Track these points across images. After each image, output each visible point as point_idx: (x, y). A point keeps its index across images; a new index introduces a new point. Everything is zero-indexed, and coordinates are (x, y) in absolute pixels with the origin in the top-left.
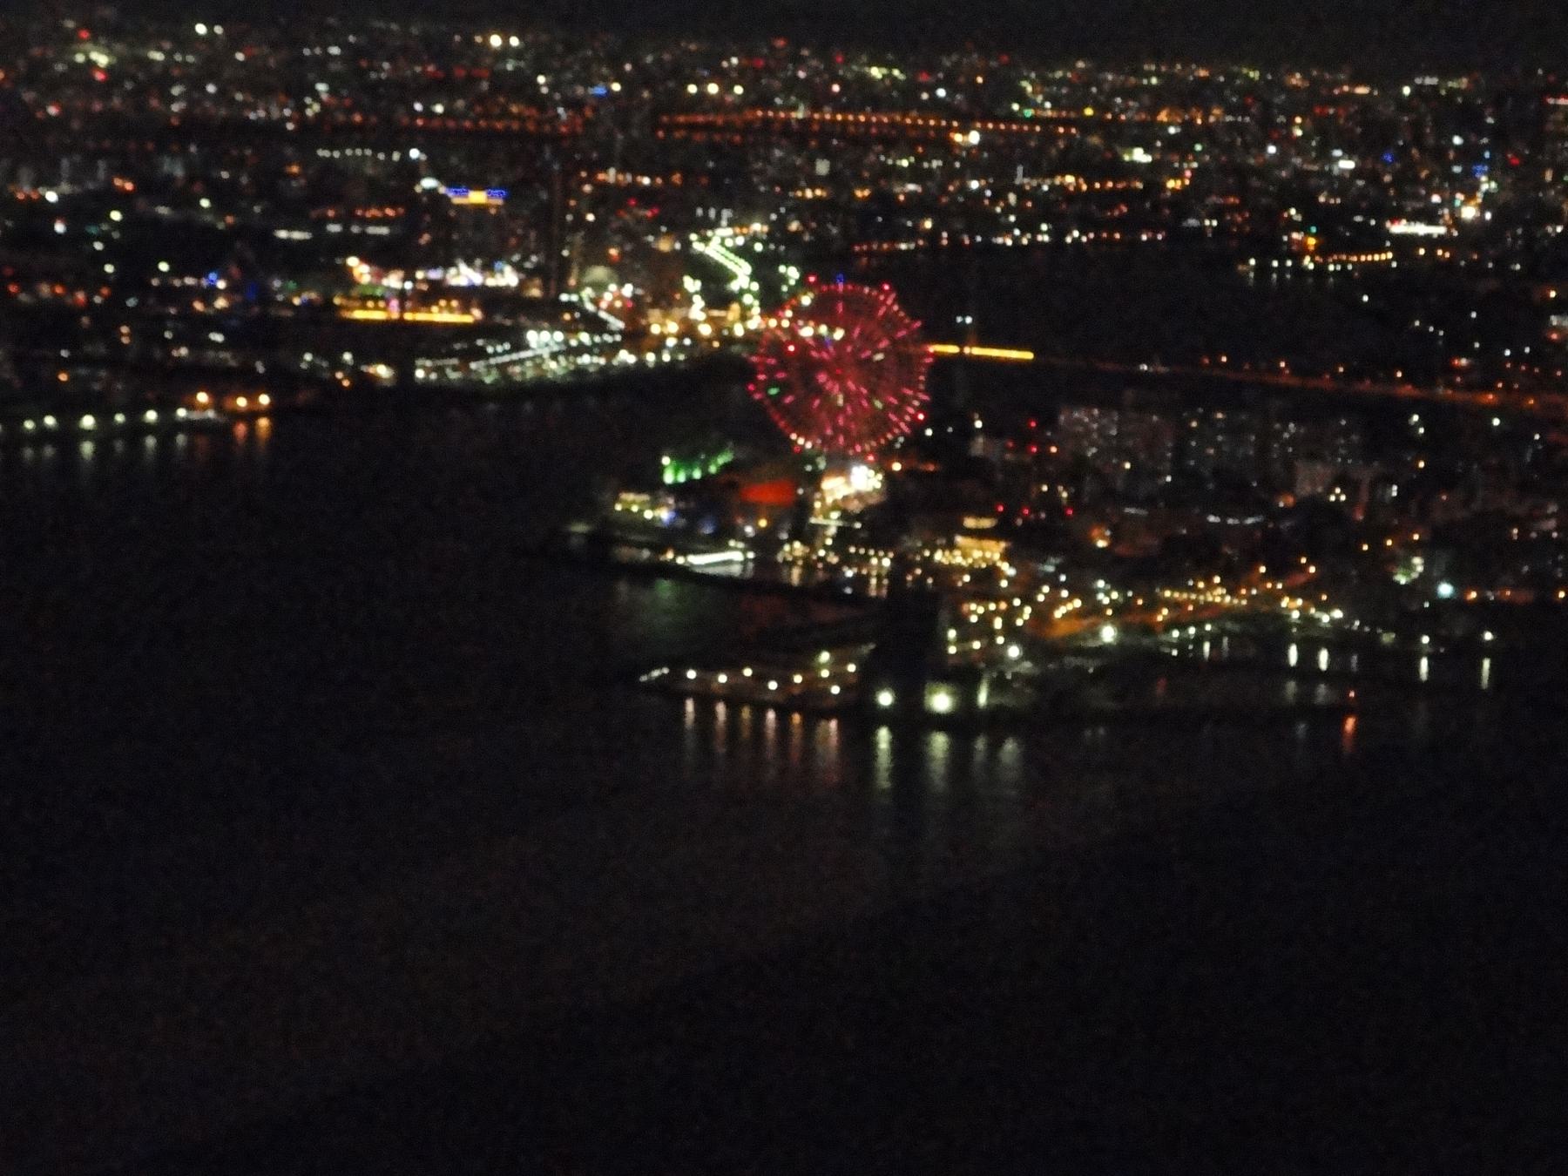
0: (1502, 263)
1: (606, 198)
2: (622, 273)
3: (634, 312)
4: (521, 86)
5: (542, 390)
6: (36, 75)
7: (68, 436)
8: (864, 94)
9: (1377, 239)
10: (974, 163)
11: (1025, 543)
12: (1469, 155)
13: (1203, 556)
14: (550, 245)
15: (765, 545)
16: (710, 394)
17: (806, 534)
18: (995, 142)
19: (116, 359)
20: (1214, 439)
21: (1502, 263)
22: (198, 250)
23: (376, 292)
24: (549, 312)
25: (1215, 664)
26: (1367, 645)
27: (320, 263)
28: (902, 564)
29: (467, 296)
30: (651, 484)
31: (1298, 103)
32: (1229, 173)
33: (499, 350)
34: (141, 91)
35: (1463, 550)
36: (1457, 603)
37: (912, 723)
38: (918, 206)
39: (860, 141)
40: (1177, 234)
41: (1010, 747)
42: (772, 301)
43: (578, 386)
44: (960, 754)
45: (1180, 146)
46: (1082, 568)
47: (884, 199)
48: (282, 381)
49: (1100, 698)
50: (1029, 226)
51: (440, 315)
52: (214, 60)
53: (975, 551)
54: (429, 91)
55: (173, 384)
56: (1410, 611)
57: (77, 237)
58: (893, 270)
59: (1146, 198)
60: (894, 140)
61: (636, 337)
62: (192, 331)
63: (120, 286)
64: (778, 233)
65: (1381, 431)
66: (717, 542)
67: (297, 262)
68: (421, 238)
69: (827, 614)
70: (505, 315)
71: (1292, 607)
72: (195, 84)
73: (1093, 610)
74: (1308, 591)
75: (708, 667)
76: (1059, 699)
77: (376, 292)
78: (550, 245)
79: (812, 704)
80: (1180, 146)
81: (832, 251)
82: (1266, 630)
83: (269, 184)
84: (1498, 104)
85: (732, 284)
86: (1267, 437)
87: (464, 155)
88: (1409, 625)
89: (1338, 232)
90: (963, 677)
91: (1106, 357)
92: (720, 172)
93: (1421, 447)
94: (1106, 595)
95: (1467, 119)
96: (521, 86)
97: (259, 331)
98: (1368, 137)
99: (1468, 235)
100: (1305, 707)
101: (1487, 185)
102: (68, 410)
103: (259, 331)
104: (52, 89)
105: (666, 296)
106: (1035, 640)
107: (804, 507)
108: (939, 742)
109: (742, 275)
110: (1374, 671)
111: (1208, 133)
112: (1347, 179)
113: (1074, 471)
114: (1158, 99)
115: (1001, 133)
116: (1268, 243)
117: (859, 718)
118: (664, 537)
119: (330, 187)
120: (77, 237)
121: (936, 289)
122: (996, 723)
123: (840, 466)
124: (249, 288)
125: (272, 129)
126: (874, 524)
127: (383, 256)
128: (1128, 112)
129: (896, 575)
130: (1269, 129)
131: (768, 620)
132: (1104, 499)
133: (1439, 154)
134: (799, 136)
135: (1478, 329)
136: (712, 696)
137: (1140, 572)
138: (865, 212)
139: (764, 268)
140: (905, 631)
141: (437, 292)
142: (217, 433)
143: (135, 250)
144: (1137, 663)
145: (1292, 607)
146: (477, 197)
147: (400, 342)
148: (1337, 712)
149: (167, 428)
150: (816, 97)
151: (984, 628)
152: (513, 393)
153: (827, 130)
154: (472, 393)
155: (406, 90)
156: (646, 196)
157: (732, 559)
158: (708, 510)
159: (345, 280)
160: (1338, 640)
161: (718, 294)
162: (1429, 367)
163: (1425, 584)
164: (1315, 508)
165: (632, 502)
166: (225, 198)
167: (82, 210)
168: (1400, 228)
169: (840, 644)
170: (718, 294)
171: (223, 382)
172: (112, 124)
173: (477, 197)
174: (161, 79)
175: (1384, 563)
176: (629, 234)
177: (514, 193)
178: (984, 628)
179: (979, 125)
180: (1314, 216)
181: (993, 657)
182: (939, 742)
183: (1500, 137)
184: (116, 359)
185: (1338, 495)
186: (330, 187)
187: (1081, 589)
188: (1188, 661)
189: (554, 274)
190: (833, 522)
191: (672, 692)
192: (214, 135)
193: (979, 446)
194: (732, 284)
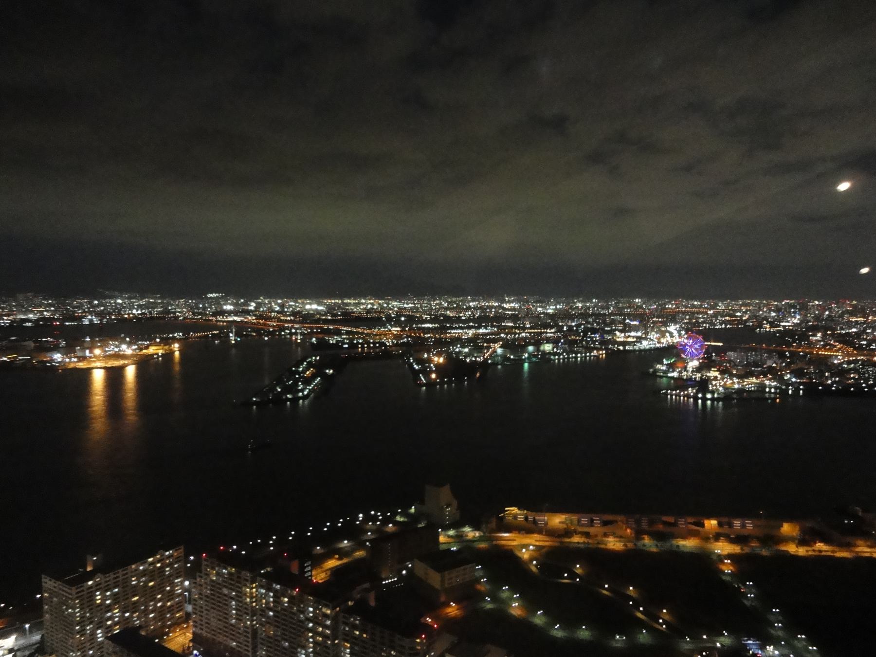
0: (802, 328)
1: (654, 322)
2: (657, 332)
3: (659, 339)
4: (641, 307)
5: (645, 350)
6: (571, 308)
7: (576, 358)
8: (693, 306)
9: (779, 326)
10: (712, 316)
11: (722, 372)
12: (795, 313)
13: (750, 374)
14: (646, 329)
15: (680, 372)
16: (672, 351)
17: (687, 371)
18: (719, 312)
19: (583, 346)
20: (752, 357)
21: (802, 328)
22: (594, 331)
23: (620, 337)
24: (646, 339)
25: (754, 391)
26: (780, 388)
27: (612, 332)
28: (702, 375)
29: (633, 337)
30: (662, 363)
31: (765, 306)
32: (754, 316)
33: (638, 345)
34: (585, 310)
35: (798, 373)
36: (796, 382)
37: (704, 400)
38: (703, 322)
39: (693, 313)
40: (746, 326)
41: (721, 403)
42: (680, 336)
43: (650, 350)
44: (712, 404)
45: (745, 312)
46: (731, 376)
47: (697, 322)
48: (607, 349)
49: (735, 396)
50: (721, 325)
51: (630, 339)
52: (596, 305)
53: (713, 373)
54: (628, 308)
55: (591, 350)
56: (788, 384)
57: (577, 330)
58: (699, 332)
59: (741, 321)
60: (699, 313)
61: (659, 342)
62: (594, 342)
63: (583, 337)
64: (681, 327)
65: (782, 356)
66: (673, 371)
67: (609, 332)
68: (626, 329)
69: (689, 383)
70: (639, 339)
71: (767, 382)
72: (593, 308)
73: (733, 383)
74: (770, 380)
75: (672, 390)
76: (728, 397)
77: (620, 337)
78: (646, 329)
79: (688, 396)
80: (745, 312)
81: (691, 329)
82: (762, 387)
83: (604, 322)
84: (799, 304)
85: (674, 335)
86: (762, 356)
87: (633, 317)
88: (788, 385)
89: (772, 325)
90: (713, 392)
91: (733, 343)
92: (672, 318)
93: (788, 358)
94: (735, 380)
95: (794, 307)
96: (641, 307)
97: (604, 343)
98: (778, 310)
99: (795, 325)
100: (770, 398)
101: (798, 317)
102: (576, 353)
103: (604, 343)
104: (573, 309)
105: (663, 336)
106: (724, 387)
107: (686, 367)
108: (709, 402)
109: (675, 333)
110: (783, 393)
111: (750, 310)
112: (773, 317)
113: (730, 361)
114: (741, 306)
115: (308, 640)
116: (760, 326)
117: (696, 398)
118: (665, 372)
119: (613, 322)
120: (577, 330)
121: (707, 335)
122: (718, 400)
123: (692, 360)
124: (602, 336)
125: (605, 314)
126: (699, 369)
127: (621, 331)
128: (737, 308)
129: (701, 378)
130: (760, 309)
131: (681, 384)
132: (735, 366)
133: (790, 313)
134: (684, 313)
135: (797, 339)
136: (673, 395)
137: (741, 377)
138: (695, 323)
139: (679, 332)
140: (703, 385)
141: (629, 336)
142: (597, 357)
143: (585, 331)
144: (741, 391)
145: (767, 382)
146: (635, 323)
147: (624, 344)
148: (775, 399)
149: (590, 356)
150: (686, 307)
151: (716, 385)
152: (640, 351)
153: (688, 312)
154: (634, 351)
155: (623, 308)
156: (661, 322)
157: (675, 374)
158: (672, 367)
159: (615, 335)
160: (776, 388)
161: (672, 336)
162: (789, 345)
163: (790, 379)
164: (770, 367)
165: (659, 366)
166: (598, 324)
167: (578, 326)
168: (783, 324)
169: (693, 387)
170: (672, 336)
171: (598, 349)
172: (581, 314)
173: (635, 323)
174: (588, 308)
175: (782, 376)
176: (658, 328)
177: (640, 322)
178: (716, 385)
179: (303, 652)
180: (768, 322)
181: (717, 390)
182: (709, 402)
183: (800, 310)
184: (583, 346)
185: (774, 365)
186: (613, 322)
187: (731, 379)
188: (749, 392)
189: (647, 333)
190: (691, 370)
191: (666, 394)
192: (597, 315)
193: (714, 358)
194: (674, 335)
